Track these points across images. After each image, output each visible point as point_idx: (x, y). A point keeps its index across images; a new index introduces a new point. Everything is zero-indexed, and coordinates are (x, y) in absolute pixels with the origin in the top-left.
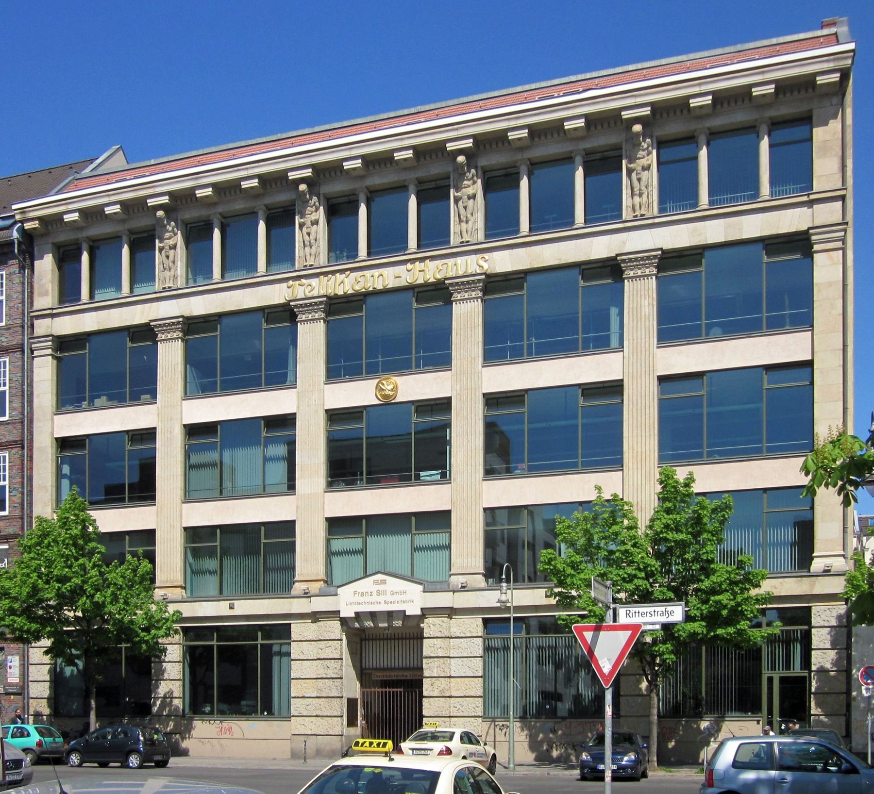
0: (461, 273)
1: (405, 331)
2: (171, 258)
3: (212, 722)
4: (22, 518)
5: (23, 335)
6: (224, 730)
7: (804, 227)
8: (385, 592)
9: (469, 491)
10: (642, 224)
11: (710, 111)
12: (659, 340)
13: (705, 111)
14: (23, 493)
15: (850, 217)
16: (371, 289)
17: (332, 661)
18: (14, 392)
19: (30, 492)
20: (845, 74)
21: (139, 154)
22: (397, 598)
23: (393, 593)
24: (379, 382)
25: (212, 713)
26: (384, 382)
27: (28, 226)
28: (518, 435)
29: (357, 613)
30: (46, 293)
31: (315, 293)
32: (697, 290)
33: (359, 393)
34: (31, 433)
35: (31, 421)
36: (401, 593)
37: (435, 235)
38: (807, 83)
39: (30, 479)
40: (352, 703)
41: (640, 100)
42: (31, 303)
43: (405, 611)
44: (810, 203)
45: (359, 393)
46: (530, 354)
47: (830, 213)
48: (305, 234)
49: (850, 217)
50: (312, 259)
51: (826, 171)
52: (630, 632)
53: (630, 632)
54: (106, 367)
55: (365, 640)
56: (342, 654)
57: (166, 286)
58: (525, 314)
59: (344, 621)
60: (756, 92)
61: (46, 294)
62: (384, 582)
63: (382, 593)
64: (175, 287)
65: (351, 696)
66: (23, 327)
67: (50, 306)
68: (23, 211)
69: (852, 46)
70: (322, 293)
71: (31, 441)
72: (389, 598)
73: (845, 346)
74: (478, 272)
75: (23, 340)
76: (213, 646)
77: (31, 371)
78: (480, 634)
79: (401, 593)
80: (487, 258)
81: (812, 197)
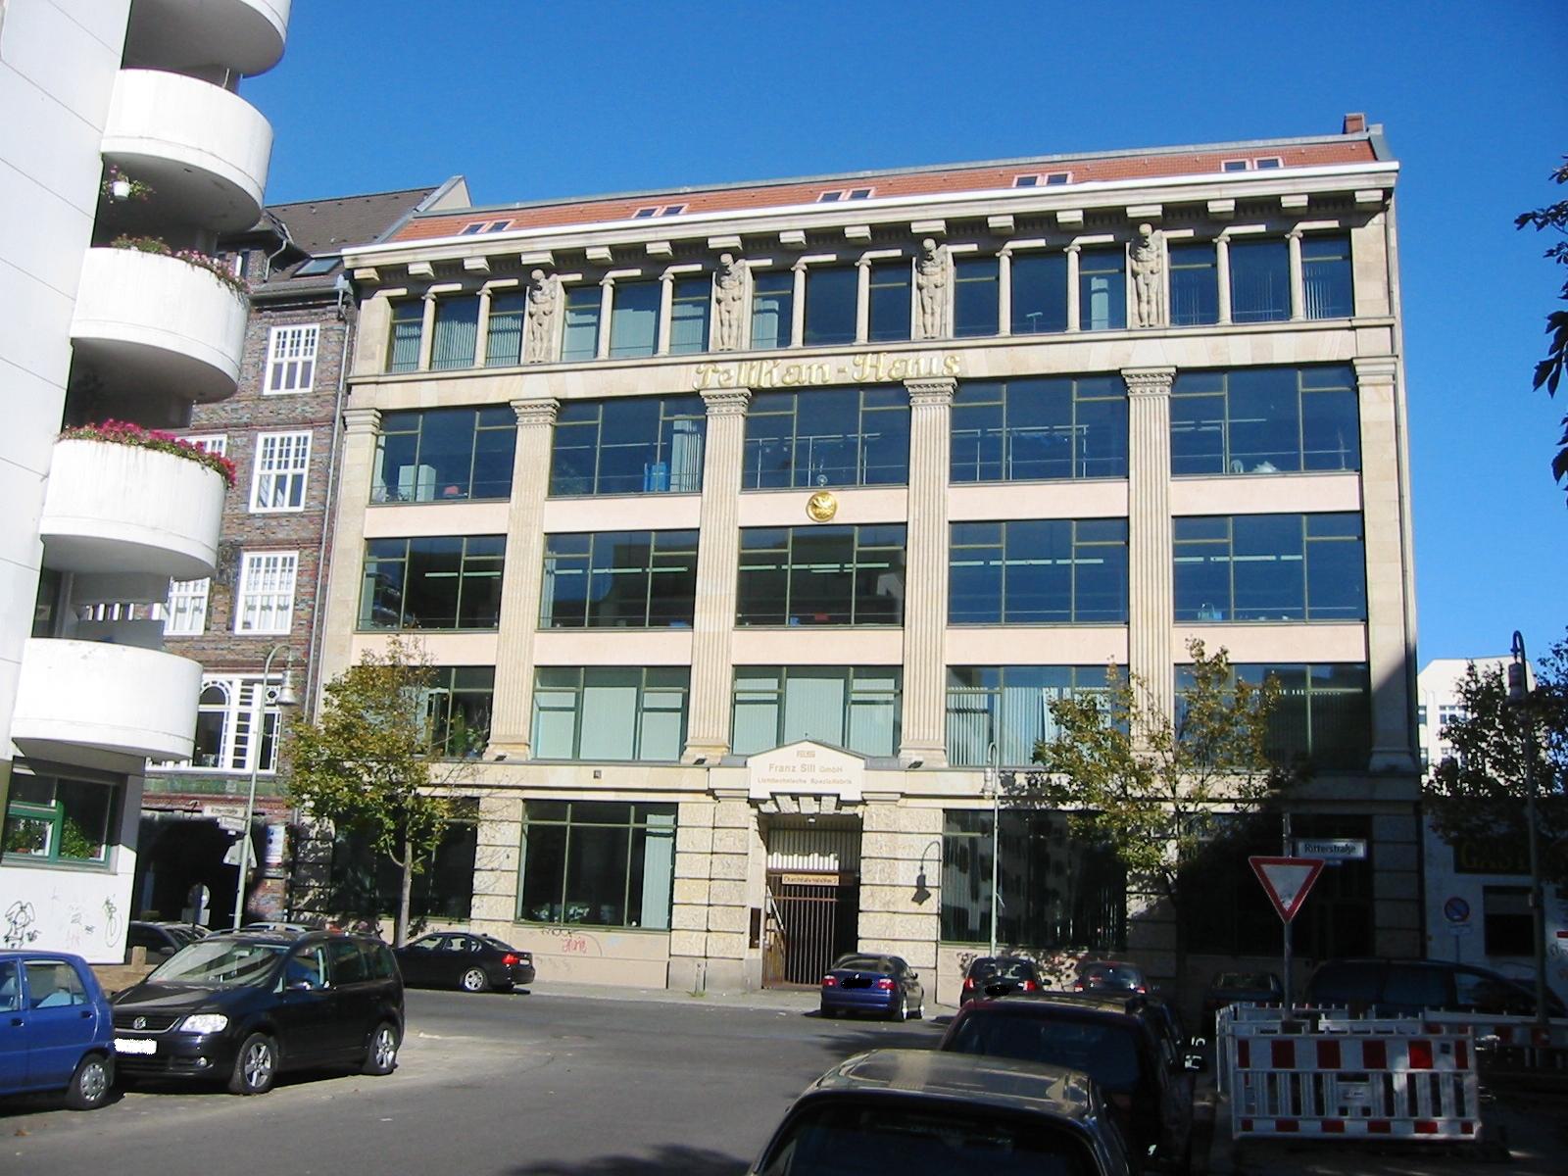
0: (923, 373)
1: (856, 434)
2: (545, 326)
3: (557, 932)
4: (309, 642)
5: (336, 406)
6: (573, 943)
7: (1349, 358)
8: (812, 768)
9: (928, 638)
10: (1149, 333)
11: (1232, 216)
12: (1172, 472)
13: (1299, 212)
14: (313, 607)
15: (1399, 350)
16: (806, 384)
17: (735, 856)
18: (315, 477)
19: (322, 606)
20: (1387, 193)
21: (492, 202)
22: (831, 776)
23: (824, 770)
24: (813, 497)
25: (551, 919)
26: (820, 498)
27: (358, 274)
28: (1010, 577)
29: (772, 794)
30: (370, 359)
31: (733, 383)
32: (1233, 418)
33: (787, 508)
34: (331, 529)
35: (333, 514)
36: (834, 770)
37: (892, 323)
38: (1348, 197)
39: (324, 588)
40: (755, 914)
41: (1148, 199)
42: (349, 368)
43: (838, 796)
44: (1353, 328)
45: (787, 508)
46: (1079, 475)
47: (1375, 342)
48: (723, 311)
49: (1399, 350)
50: (733, 341)
51: (1369, 293)
52: (1311, 867)
53: (1311, 867)
54: (464, 450)
55: (774, 829)
56: (747, 848)
57: (535, 360)
58: (1015, 430)
59: (753, 803)
60: (1286, 202)
61: (373, 356)
62: (812, 754)
63: (811, 771)
64: (738, 349)
65: (755, 906)
66: (336, 396)
67: (376, 373)
68: (355, 257)
69: (1395, 165)
70: (743, 382)
71: (330, 540)
72: (818, 775)
73: (1401, 496)
74: (945, 373)
75: (335, 412)
76: (565, 827)
77: (340, 450)
78: (940, 831)
79: (834, 770)
80: (958, 359)
81: (1355, 323)
